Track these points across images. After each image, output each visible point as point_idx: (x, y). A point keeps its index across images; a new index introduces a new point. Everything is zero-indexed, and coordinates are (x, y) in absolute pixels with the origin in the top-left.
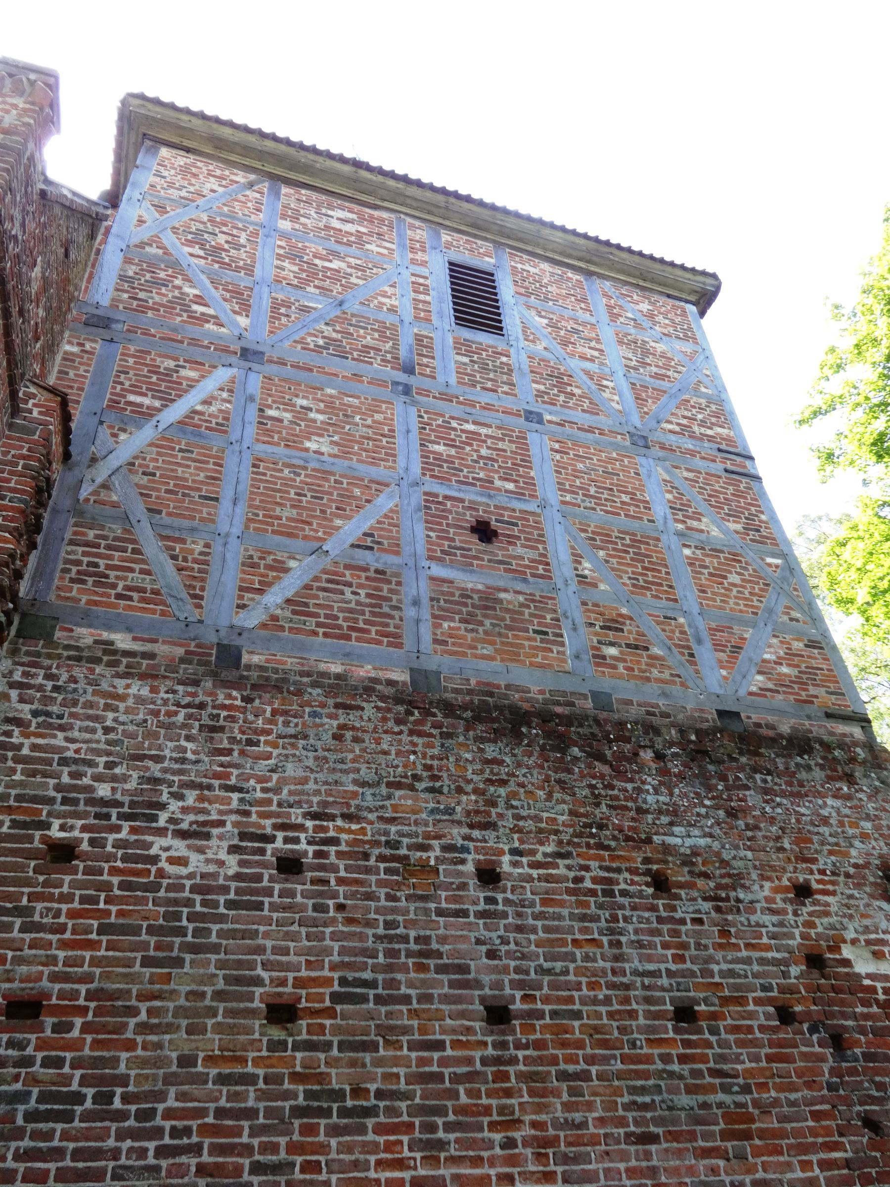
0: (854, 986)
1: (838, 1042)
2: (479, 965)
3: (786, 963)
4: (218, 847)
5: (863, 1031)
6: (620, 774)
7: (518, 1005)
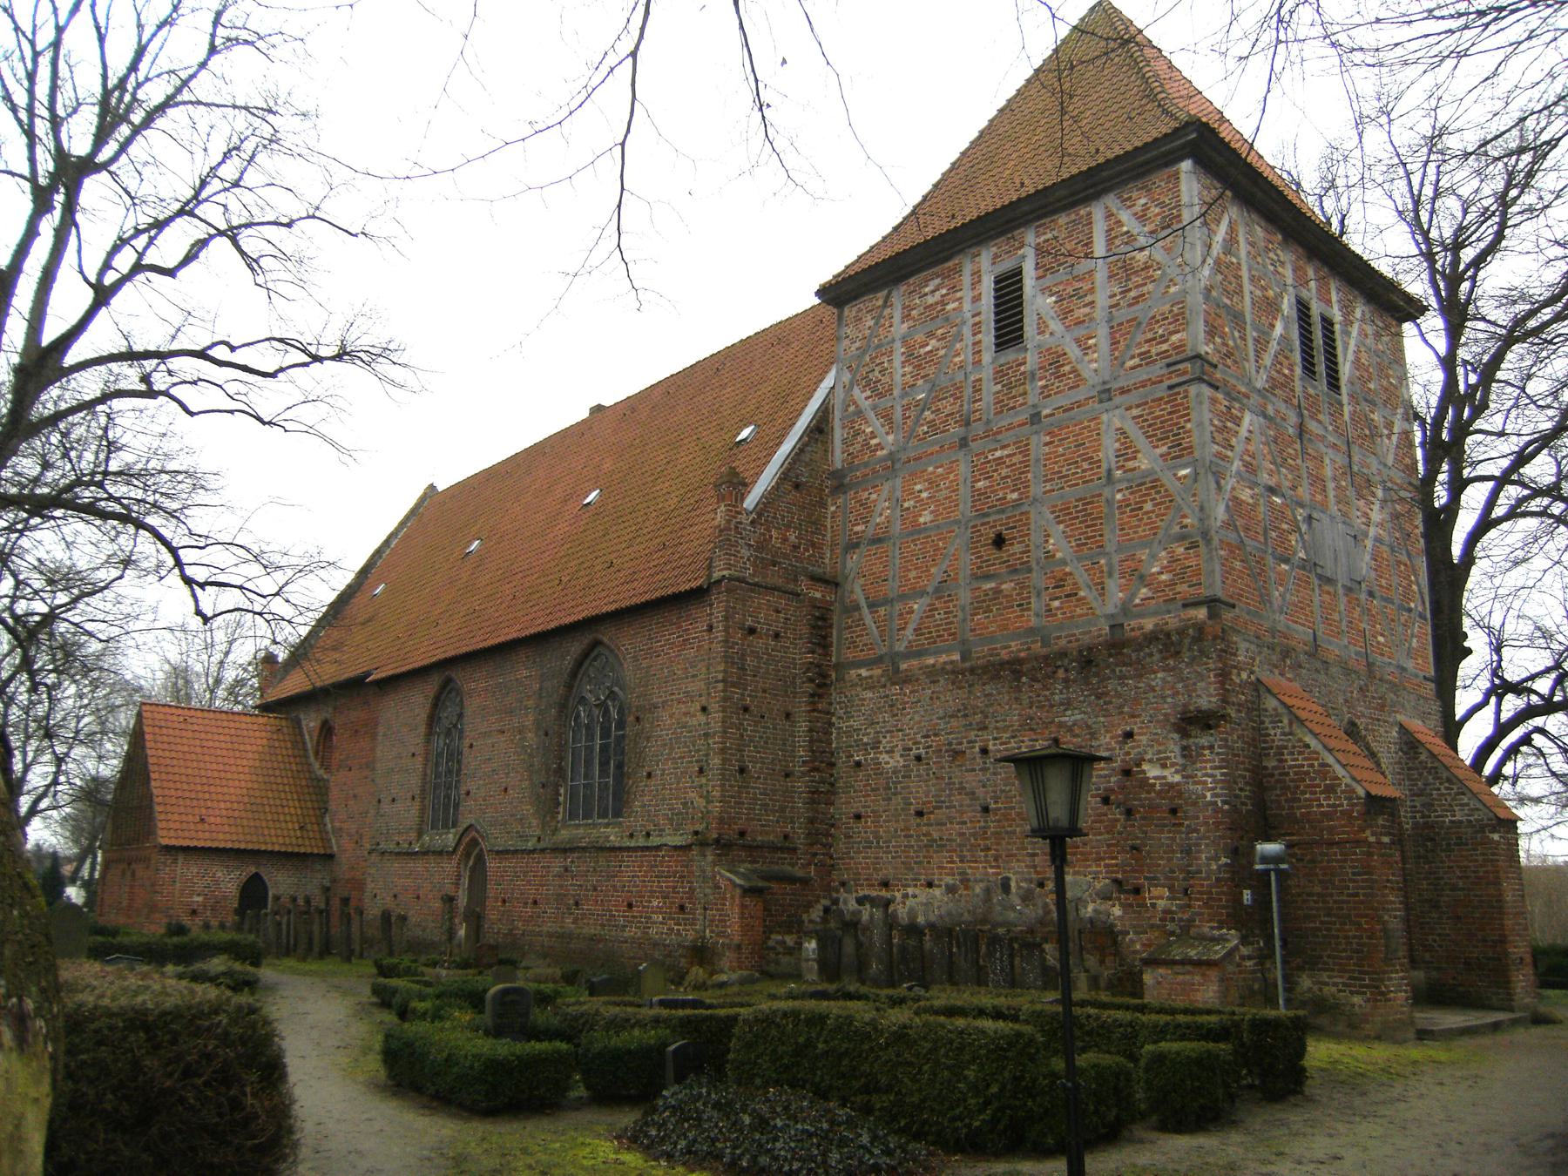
0: (1144, 783)
1: (1129, 812)
2: (980, 792)
3: (1109, 776)
4: (897, 756)
5: (1143, 806)
6: (1045, 688)
7: (993, 806)
